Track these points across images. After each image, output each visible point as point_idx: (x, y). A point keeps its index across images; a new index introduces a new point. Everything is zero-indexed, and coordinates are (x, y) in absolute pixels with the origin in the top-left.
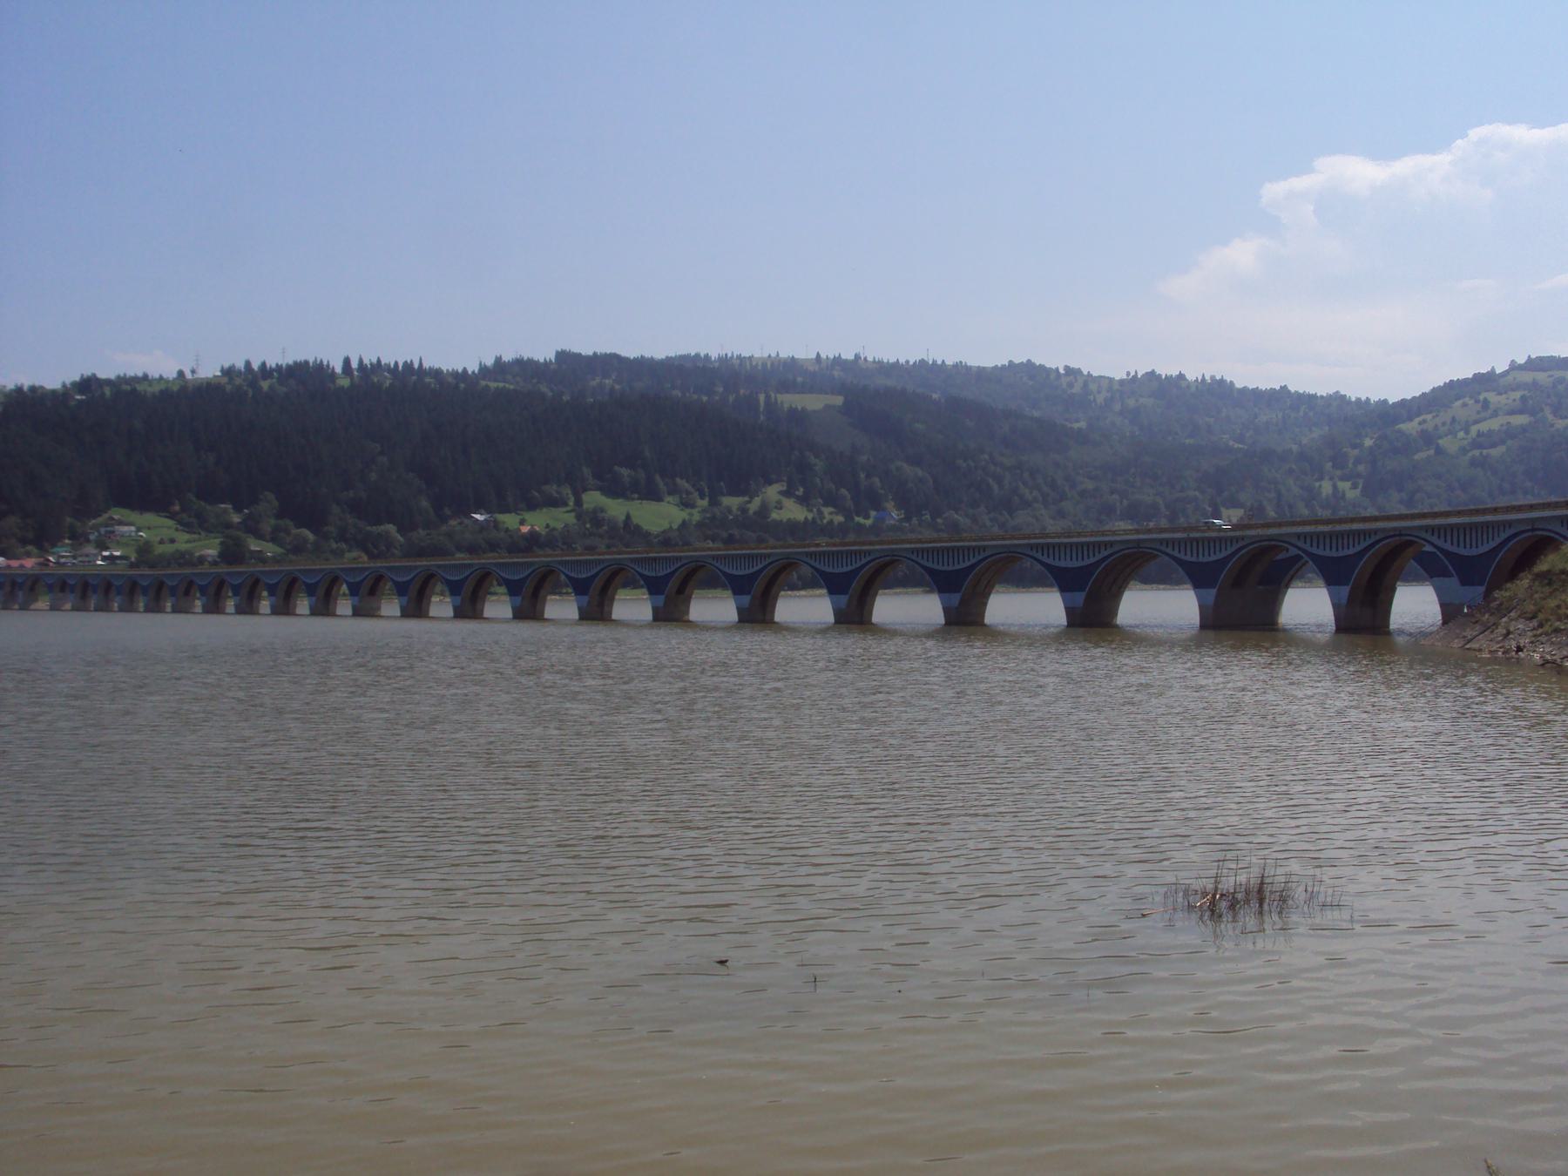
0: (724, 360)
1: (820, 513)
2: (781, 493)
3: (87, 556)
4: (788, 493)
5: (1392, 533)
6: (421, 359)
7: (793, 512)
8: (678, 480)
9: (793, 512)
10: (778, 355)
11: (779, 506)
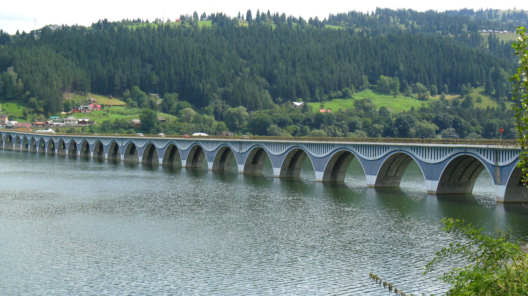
0: (334, 19)
1: (503, 105)
2: (480, 93)
3: (70, 121)
4: (486, 93)
5: (386, 169)
6: (243, 15)
7: (487, 103)
8: (418, 84)
9: (487, 103)
10: (77, 24)
11: (479, 101)
